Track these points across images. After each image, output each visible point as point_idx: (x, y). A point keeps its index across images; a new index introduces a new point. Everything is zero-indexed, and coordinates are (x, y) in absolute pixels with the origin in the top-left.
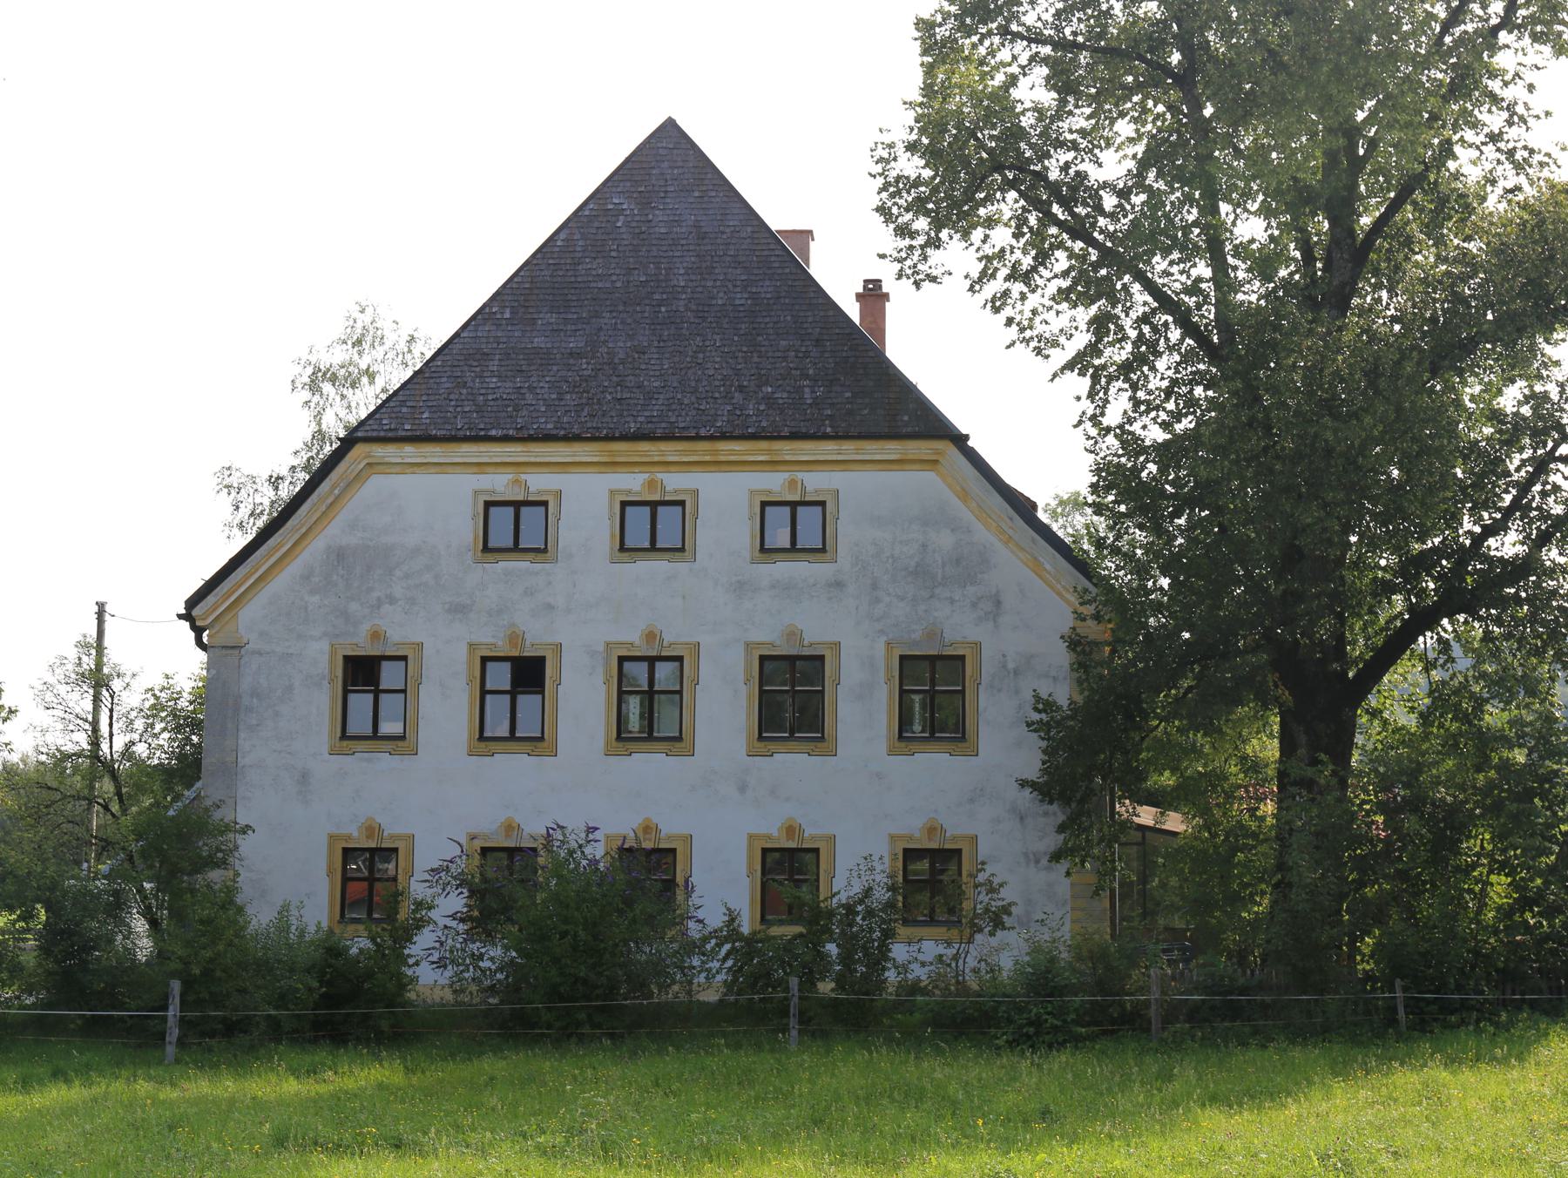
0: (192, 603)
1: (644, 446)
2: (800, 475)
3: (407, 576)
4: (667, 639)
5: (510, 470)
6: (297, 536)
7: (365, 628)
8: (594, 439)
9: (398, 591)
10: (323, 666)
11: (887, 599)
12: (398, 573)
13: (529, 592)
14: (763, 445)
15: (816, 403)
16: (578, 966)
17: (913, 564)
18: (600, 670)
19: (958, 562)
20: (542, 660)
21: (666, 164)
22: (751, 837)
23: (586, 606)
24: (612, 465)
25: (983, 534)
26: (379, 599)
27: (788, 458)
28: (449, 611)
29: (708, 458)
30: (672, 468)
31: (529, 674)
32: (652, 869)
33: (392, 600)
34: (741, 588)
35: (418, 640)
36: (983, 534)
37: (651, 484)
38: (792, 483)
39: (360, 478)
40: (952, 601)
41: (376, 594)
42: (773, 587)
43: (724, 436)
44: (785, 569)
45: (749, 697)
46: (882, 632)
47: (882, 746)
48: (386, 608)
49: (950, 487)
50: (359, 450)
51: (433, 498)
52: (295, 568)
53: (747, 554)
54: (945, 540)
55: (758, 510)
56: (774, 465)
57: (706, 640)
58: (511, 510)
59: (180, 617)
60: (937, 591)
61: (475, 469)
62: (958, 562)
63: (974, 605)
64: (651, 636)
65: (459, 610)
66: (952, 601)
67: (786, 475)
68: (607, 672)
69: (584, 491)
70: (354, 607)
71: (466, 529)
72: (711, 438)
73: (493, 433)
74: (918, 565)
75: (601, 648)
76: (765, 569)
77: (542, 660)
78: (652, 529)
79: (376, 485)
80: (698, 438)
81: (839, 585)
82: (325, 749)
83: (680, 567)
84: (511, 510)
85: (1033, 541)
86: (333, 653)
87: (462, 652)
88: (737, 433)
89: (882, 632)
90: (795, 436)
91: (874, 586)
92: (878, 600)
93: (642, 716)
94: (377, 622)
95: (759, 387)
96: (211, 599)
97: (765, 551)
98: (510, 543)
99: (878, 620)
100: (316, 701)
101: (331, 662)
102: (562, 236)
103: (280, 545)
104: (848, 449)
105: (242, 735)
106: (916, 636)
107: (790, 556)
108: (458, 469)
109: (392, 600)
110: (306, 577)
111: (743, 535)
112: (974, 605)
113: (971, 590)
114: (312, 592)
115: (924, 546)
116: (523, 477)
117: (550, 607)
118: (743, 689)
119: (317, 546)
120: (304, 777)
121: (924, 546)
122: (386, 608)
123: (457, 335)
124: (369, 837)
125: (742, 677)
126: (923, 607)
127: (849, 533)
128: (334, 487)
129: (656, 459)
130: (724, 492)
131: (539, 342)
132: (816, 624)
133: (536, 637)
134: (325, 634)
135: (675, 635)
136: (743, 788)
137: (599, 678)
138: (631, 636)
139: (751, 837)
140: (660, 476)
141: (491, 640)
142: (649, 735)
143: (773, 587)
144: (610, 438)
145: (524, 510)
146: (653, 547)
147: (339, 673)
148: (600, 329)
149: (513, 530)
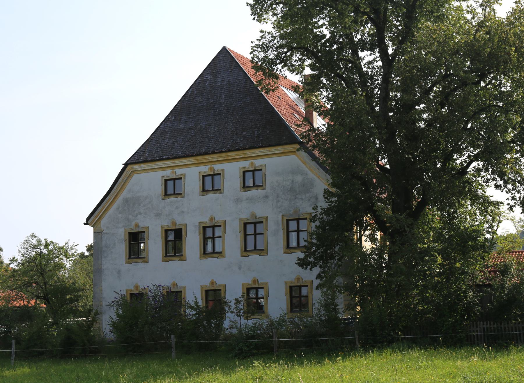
0: (88, 219)
1: (207, 157)
2: (254, 161)
3: (144, 206)
4: (217, 219)
5: (171, 168)
6: (114, 196)
7: (133, 223)
8: (192, 156)
9: (142, 211)
10: (123, 236)
11: (282, 200)
12: (142, 205)
13: (177, 208)
14: (241, 152)
15: (258, 137)
16: (159, 327)
17: (289, 187)
18: (198, 232)
19: (304, 185)
20: (181, 229)
21: (222, 62)
22: (243, 284)
23: (193, 211)
24: (199, 164)
25: (311, 175)
26: (137, 214)
27: (249, 156)
28: (156, 216)
29: (225, 158)
30: (217, 163)
31: (179, 233)
32: (174, 296)
33: (140, 214)
34: (238, 201)
35: (147, 226)
36: (311, 175)
37: (211, 169)
38: (252, 164)
39: (130, 176)
40: (302, 199)
41: (136, 212)
42: (247, 199)
43: (230, 151)
44: (250, 193)
45: (241, 237)
46: (280, 212)
47: (282, 251)
48: (139, 216)
49: (300, 160)
50: (129, 167)
51: (151, 179)
52: (115, 206)
53: (239, 189)
54: (299, 178)
55: (242, 174)
56: (246, 158)
57: (228, 219)
58: (211, 177)
59: (85, 224)
60: (297, 196)
61: (161, 169)
62: (304, 185)
63: (309, 200)
64: (212, 219)
65: (158, 215)
66: (302, 199)
67: (250, 161)
68: (200, 232)
69: (191, 173)
70: (130, 217)
71: (159, 189)
72: (226, 152)
73: (164, 157)
74: (291, 188)
75: (198, 224)
76: (244, 193)
77: (181, 229)
78: (210, 184)
79: (135, 177)
80: (222, 152)
81: (267, 197)
82: (124, 262)
83: (220, 195)
84: (211, 177)
85: (326, 176)
86: (125, 232)
87: (159, 229)
88: (233, 149)
89: (280, 212)
90: (250, 148)
91: (278, 196)
92: (279, 201)
93: (207, 244)
94: (137, 221)
95: (242, 133)
96: (92, 218)
97: (244, 187)
98: (173, 192)
99: (279, 208)
100: (121, 249)
101: (125, 235)
102: (191, 90)
103: (110, 199)
104: (267, 151)
105: (103, 259)
106: (291, 212)
107: (173, 196)
108: (157, 170)
109: (140, 214)
110: (118, 209)
111: (238, 183)
112: (309, 200)
113: (308, 195)
114: (120, 213)
115: (293, 181)
116: (175, 170)
117: (183, 212)
118: (239, 234)
119: (120, 199)
120: (119, 272)
121: (293, 181)
122: (139, 216)
123: (159, 127)
124: (137, 289)
125: (238, 231)
126: (293, 202)
127: (270, 180)
128: (123, 180)
129: (211, 160)
130: (231, 169)
131: (182, 126)
132: (261, 210)
133: (180, 221)
134: (123, 226)
135: (219, 218)
136: (240, 268)
137: (197, 234)
138: (206, 219)
139: (243, 284)
140: (213, 166)
141: (167, 224)
142: (256, 250)
143: (247, 199)
144: (197, 155)
145: (256, 173)
146: (213, 190)
147: (127, 238)
148: (199, 119)
149: (172, 188)
